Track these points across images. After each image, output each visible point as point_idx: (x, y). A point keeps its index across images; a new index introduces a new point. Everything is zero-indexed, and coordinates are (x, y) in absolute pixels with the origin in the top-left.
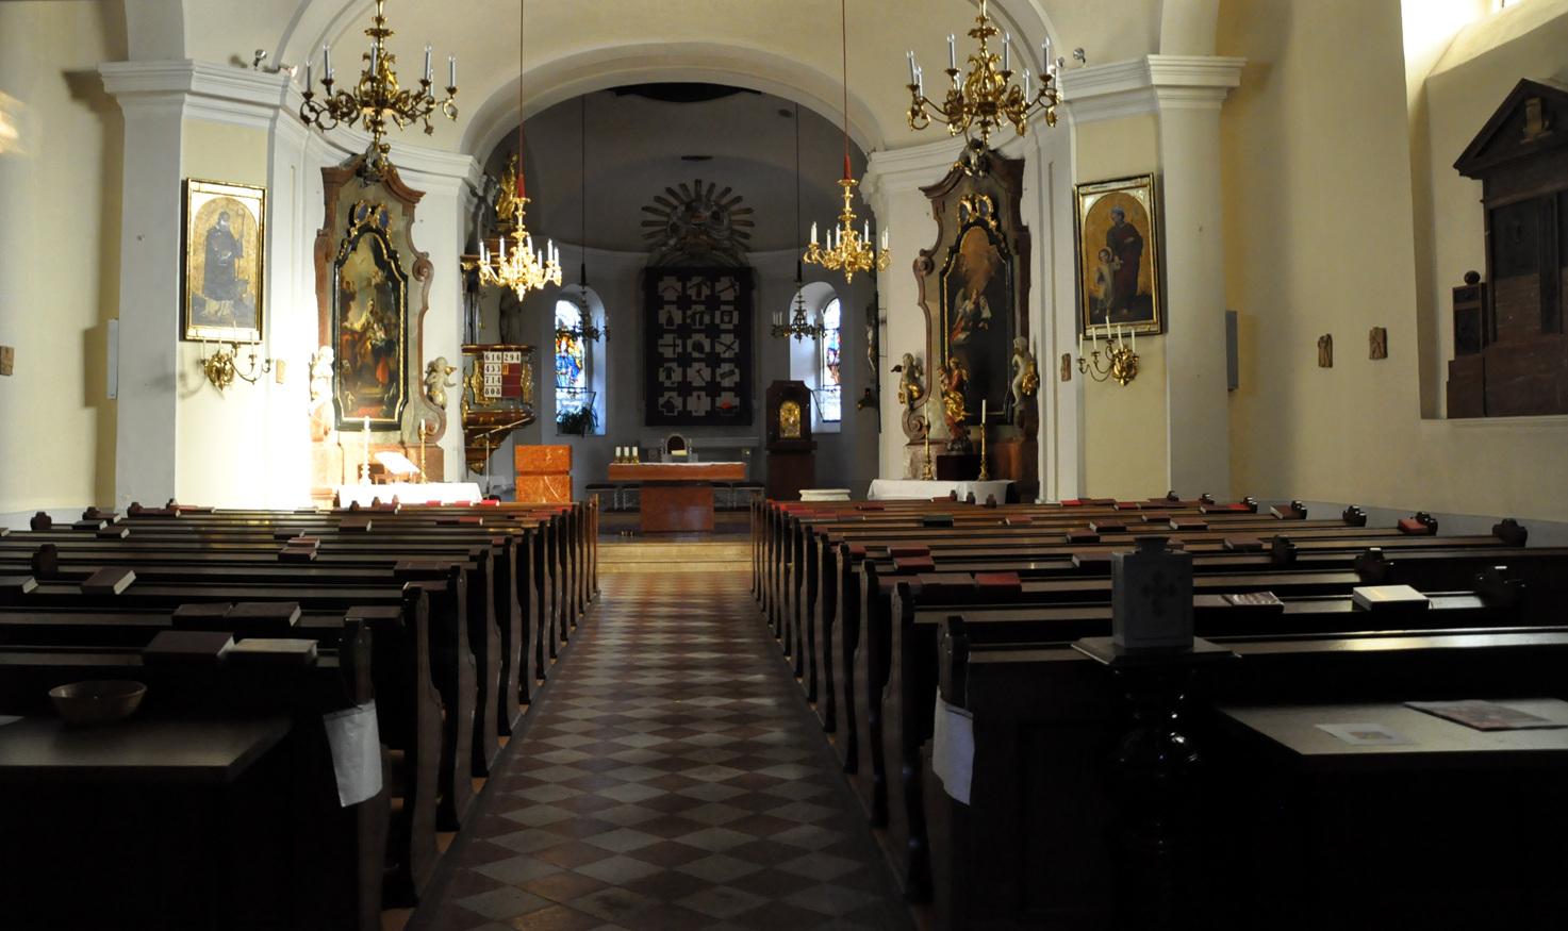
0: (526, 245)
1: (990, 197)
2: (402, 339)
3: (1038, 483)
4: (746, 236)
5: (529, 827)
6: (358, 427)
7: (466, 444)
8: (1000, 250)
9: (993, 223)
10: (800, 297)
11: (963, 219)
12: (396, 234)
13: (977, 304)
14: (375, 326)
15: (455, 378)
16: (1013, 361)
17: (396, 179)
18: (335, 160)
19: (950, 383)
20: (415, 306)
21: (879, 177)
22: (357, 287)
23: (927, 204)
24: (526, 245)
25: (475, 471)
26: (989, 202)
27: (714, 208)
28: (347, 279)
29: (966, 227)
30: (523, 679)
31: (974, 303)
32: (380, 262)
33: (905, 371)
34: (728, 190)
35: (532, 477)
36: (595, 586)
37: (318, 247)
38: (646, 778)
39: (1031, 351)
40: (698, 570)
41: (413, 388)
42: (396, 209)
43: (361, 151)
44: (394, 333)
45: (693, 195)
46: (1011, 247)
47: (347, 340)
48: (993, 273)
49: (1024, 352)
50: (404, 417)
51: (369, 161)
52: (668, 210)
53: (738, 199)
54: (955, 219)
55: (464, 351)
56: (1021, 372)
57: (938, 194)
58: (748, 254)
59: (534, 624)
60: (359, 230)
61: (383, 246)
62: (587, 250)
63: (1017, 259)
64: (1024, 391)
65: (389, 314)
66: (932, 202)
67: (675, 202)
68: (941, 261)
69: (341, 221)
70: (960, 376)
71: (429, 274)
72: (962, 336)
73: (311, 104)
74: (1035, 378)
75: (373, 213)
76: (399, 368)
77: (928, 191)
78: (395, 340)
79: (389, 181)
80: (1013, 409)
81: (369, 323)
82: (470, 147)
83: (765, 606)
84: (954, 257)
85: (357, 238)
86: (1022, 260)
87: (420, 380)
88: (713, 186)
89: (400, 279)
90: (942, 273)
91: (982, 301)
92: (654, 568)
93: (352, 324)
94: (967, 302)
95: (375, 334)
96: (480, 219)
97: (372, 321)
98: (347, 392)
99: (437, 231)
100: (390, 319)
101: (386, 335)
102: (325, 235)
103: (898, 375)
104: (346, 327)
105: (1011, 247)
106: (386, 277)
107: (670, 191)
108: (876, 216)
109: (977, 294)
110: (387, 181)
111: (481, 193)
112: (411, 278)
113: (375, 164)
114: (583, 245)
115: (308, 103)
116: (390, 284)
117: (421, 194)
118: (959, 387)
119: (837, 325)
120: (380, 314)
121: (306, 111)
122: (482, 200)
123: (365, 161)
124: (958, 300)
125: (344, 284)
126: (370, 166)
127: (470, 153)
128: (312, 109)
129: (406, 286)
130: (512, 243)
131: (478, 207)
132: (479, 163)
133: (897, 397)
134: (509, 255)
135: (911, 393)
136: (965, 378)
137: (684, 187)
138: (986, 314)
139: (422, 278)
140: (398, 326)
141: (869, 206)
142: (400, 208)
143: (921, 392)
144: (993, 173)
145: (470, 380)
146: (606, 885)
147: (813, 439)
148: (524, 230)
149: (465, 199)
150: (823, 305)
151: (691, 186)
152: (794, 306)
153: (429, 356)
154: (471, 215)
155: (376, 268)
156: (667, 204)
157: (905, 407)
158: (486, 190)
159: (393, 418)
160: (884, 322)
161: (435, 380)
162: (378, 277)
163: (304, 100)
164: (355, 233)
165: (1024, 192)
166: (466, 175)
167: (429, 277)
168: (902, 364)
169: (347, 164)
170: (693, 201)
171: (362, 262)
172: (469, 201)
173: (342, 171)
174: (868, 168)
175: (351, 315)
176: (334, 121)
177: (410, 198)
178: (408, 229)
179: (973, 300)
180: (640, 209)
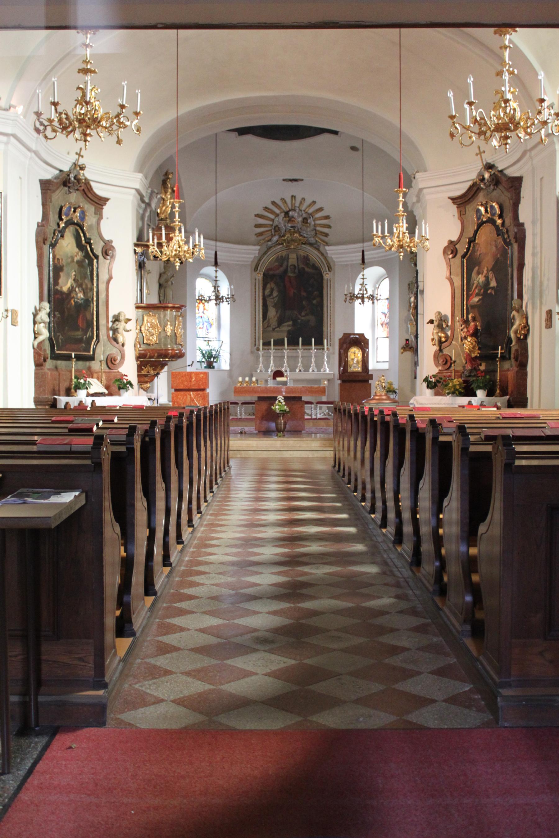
0: (180, 232)
1: (498, 203)
2: (95, 299)
3: (527, 399)
4: (326, 235)
5: (201, 598)
6: (68, 358)
7: (138, 372)
8: (504, 240)
9: (499, 222)
10: (363, 275)
11: (478, 218)
12: (90, 227)
13: (487, 277)
14: (77, 289)
15: (131, 325)
16: (512, 315)
17: (90, 189)
18: (49, 174)
19: (468, 331)
20: (104, 277)
21: (421, 190)
22: (64, 263)
23: (454, 209)
24: (180, 232)
25: (144, 390)
26: (496, 207)
27: (304, 215)
28: (57, 257)
29: (480, 226)
30: (166, 547)
31: (485, 276)
32: (80, 246)
33: (436, 323)
34: (314, 202)
35: (182, 393)
36: (228, 463)
37: (38, 234)
38: (276, 571)
39: (524, 308)
40: (294, 456)
41: (103, 332)
42: (90, 209)
43: (66, 169)
44: (90, 294)
45: (290, 206)
46: (512, 237)
47: (58, 298)
48: (499, 256)
49: (519, 309)
50: (97, 351)
51: (72, 176)
52: (272, 217)
53: (321, 209)
54: (473, 218)
55: (137, 308)
56: (517, 323)
57: (462, 202)
58: (327, 248)
59: (186, 486)
60: (66, 223)
61: (82, 235)
62: (218, 244)
63: (515, 246)
64: (519, 336)
65: (86, 281)
66: (457, 207)
67: (277, 211)
68: (462, 249)
69: (53, 217)
70: (476, 326)
71: (113, 255)
72: (476, 299)
73: (41, 120)
74: (526, 327)
75: (74, 211)
76: (93, 319)
77: (454, 199)
78: (90, 299)
79: (86, 190)
80: (510, 348)
81: (72, 287)
82: (140, 168)
83: (344, 474)
84: (472, 244)
85: (64, 228)
86: (519, 246)
87: (108, 327)
88: (304, 199)
89: (93, 257)
90: (464, 255)
91: (491, 275)
92: (265, 455)
93: (61, 288)
94: (480, 276)
95: (77, 294)
96: (146, 219)
97: (75, 286)
98: (58, 334)
99: (118, 226)
100: (86, 285)
101: (84, 295)
102: (43, 226)
103: (431, 326)
104: (57, 290)
105: (512, 237)
106: (84, 256)
107: (273, 203)
108: (417, 218)
109: (487, 270)
110: (83, 190)
111: (147, 200)
112: (101, 257)
113: (75, 178)
114: (216, 241)
115: (38, 120)
116: (87, 261)
117: (107, 200)
118: (475, 334)
119: (387, 296)
120: (80, 281)
121: (38, 125)
122: (148, 205)
123: (69, 175)
124: (474, 275)
125: (56, 260)
126: (72, 179)
127: (140, 171)
128: (41, 124)
129: (97, 262)
130: (170, 229)
131: (145, 210)
132: (146, 178)
133: (431, 341)
134: (169, 239)
135: (440, 338)
136: (479, 328)
137: (283, 200)
138: (493, 284)
139: (108, 257)
140: (92, 289)
141: (412, 212)
142: (93, 209)
143: (447, 337)
144: (500, 187)
145: (141, 328)
146: (255, 630)
147: (370, 373)
148: (179, 222)
149: (136, 204)
150: (379, 281)
151: (289, 201)
152: (359, 281)
153: (112, 312)
154: (140, 216)
155: (77, 250)
156: (272, 212)
157: (436, 348)
158: (151, 198)
159: (90, 352)
160: (422, 292)
161: (118, 327)
162: (79, 256)
163: (35, 117)
164: (62, 225)
165: (522, 199)
166: (138, 186)
167: (113, 257)
168: (434, 319)
169: (56, 177)
170: (290, 210)
171: (68, 245)
172: (139, 206)
173: (53, 182)
174: (413, 185)
175: (60, 281)
176: (54, 134)
177: (100, 202)
178: (98, 224)
179: (484, 274)
180: (253, 216)
